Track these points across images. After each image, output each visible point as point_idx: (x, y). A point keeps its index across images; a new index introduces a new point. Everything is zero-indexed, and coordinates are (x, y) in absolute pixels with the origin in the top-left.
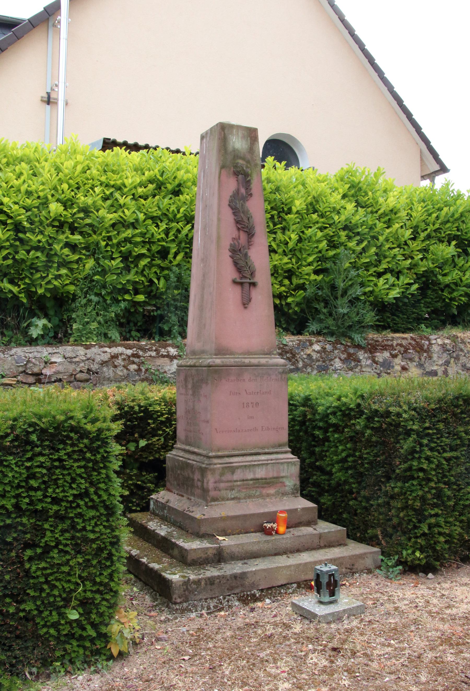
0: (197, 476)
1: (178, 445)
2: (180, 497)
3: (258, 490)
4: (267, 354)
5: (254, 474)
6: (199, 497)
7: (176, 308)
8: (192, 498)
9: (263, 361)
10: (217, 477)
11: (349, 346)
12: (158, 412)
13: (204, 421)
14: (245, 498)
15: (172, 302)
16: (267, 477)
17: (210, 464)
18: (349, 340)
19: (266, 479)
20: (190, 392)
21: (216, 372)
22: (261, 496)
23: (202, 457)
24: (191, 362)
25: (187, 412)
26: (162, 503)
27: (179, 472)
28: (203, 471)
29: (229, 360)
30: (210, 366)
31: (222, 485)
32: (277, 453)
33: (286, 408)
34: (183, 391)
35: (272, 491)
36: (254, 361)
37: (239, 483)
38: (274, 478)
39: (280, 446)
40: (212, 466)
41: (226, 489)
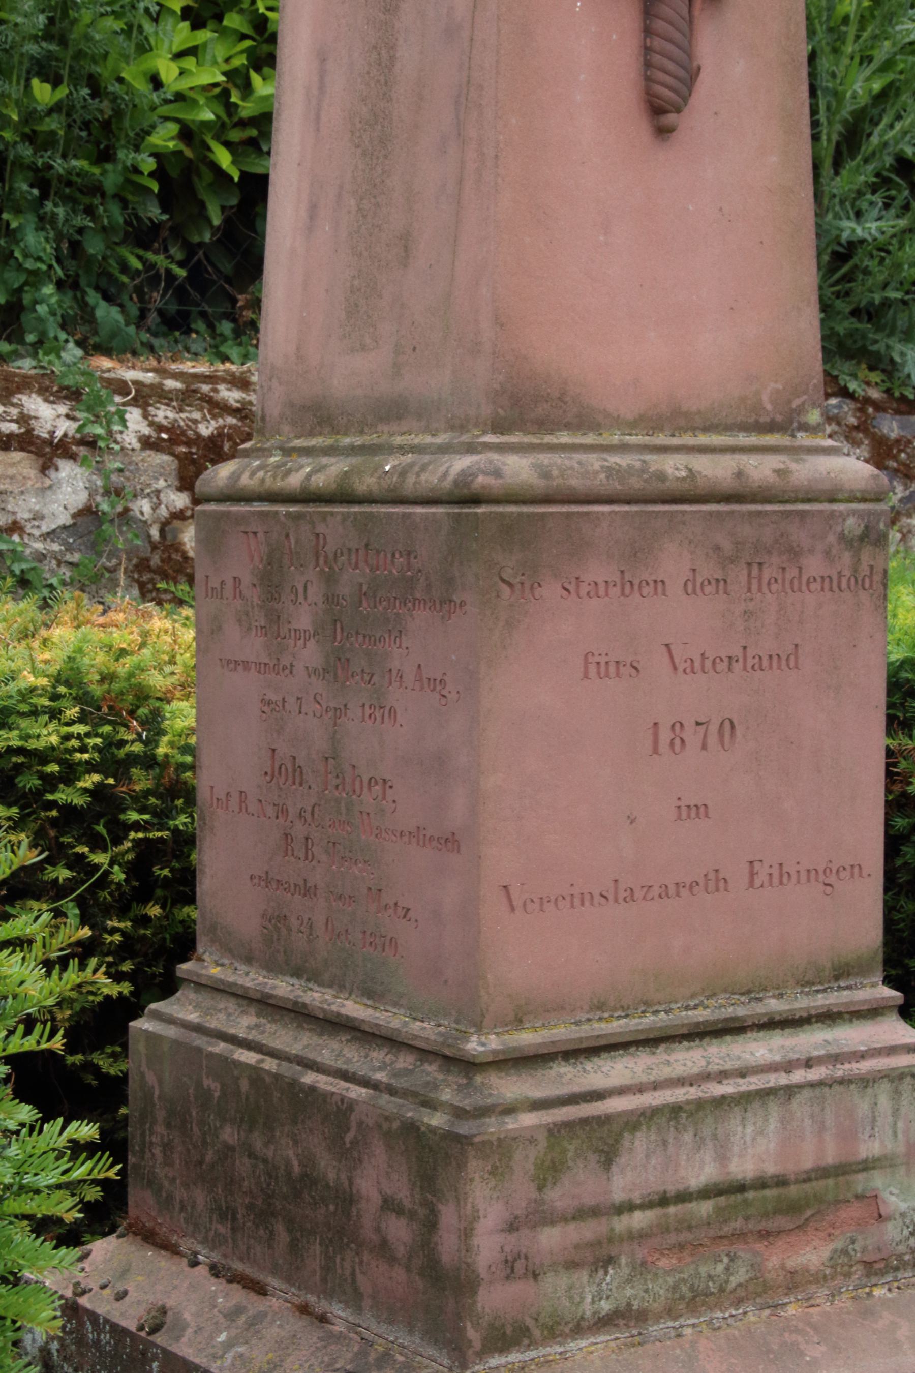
0: (378, 1178)
1: (208, 965)
2: (238, 1295)
3: (740, 1249)
4: (771, 427)
5: (722, 1158)
6: (391, 1313)
7: (43, 182)
8: (337, 1310)
9: (761, 469)
10: (522, 1190)
11: (879, 407)
12: (43, 756)
13: (419, 836)
14: (670, 1312)
15: (26, 151)
16: (790, 1168)
17: (483, 1112)
18: (876, 377)
19: (781, 1182)
20: (310, 654)
21: (490, 539)
22: (761, 1291)
23: (405, 1061)
24: (328, 472)
25: (283, 771)
26: (118, 1331)
27: (229, 1135)
28: (435, 1159)
29: (583, 464)
30: (476, 500)
31: (550, 1239)
32: (829, 1017)
33: (883, 753)
34: (253, 647)
35: (812, 1254)
36: (716, 470)
37: (639, 1219)
38: (823, 1172)
39: (843, 972)
40: (492, 1127)
41: (572, 1265)
